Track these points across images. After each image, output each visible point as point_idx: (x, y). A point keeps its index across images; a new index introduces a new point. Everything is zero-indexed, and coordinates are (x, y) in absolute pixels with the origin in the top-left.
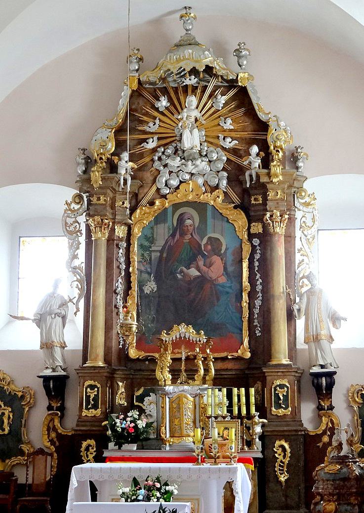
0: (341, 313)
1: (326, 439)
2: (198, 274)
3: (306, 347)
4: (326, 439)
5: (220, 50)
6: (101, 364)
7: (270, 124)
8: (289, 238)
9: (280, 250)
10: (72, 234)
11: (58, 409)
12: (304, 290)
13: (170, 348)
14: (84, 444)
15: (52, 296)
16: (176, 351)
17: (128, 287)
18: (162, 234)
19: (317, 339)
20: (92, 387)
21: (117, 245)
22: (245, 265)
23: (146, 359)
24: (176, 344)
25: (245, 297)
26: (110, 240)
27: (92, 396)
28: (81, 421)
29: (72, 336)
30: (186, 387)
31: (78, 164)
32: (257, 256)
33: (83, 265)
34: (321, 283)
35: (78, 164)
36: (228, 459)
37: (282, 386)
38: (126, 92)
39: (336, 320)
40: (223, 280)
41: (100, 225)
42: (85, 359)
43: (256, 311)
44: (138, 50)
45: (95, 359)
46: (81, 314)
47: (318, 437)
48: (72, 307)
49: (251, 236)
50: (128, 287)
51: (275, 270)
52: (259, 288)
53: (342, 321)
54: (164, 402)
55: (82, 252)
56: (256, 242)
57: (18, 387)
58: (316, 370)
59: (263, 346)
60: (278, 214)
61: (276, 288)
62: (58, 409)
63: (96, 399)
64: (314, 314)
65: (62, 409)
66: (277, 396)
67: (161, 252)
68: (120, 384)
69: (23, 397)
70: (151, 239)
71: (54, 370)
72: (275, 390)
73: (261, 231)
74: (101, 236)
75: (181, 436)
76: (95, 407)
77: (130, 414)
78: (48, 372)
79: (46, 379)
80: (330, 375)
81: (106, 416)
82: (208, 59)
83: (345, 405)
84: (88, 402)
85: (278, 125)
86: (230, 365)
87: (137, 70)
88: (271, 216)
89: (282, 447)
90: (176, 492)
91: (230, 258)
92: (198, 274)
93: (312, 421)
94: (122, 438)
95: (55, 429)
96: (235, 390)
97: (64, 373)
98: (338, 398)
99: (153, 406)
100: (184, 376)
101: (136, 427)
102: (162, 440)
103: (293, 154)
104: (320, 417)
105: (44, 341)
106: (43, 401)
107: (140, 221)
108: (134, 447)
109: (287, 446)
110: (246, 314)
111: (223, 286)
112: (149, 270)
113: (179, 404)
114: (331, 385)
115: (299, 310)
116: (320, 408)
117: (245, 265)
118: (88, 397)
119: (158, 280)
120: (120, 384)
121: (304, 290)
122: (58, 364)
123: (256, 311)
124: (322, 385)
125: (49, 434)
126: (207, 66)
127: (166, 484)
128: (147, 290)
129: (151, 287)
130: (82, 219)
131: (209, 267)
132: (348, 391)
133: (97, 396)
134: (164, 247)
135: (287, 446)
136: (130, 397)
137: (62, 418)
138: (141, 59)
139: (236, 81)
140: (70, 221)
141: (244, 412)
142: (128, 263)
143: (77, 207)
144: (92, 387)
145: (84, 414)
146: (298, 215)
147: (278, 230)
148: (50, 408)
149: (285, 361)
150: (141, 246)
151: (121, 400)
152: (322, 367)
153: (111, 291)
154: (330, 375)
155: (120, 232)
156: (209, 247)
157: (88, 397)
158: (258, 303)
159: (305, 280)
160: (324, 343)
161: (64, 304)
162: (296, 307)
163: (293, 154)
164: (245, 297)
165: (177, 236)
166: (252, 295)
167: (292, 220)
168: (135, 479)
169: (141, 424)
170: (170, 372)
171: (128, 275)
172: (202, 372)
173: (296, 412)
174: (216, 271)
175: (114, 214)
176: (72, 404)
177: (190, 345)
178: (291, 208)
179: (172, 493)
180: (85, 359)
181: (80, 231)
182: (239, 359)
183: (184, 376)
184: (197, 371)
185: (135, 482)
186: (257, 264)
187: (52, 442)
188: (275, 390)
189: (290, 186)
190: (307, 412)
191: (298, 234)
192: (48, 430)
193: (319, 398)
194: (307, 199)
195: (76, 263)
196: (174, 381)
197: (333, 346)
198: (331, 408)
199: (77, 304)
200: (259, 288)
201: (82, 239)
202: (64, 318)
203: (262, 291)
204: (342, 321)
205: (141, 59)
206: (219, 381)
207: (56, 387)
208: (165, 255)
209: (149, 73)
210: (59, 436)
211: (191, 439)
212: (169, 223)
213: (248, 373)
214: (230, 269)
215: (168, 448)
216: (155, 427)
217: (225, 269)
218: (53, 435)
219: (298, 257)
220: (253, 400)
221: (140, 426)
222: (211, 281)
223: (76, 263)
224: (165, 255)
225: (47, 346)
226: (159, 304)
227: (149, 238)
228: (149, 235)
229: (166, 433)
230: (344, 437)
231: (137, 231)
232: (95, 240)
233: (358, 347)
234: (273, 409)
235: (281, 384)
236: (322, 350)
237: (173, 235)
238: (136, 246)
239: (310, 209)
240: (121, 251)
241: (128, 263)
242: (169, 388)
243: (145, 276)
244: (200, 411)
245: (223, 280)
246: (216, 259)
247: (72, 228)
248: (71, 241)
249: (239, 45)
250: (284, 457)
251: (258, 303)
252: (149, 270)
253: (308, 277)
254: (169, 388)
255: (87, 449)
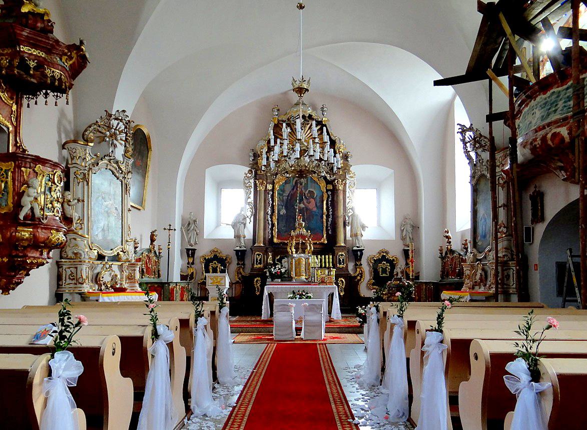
0: (366, 224)
1: (359, 278)
2: (304, 206)
3: (351, 239)
4: (359, 278)
5: (314, 109)
6: (262, 245)
7: (336, 141)
8: (344, 191)
9: (341, 197)
10: (249, 187)
11: (242, 264)
12: (350, 214)
13: (295, 238)
14: (256, 280)
15: (239, 215)
16: (297, 239)
17: (273, 211)
18: (288, 188)
19: (356, 235)
20: (259, 255)
21: (268, 193)
22: (325, 202)
23: (281, 243)
24: (298, 236)
25: (325, 217)
26: (265, 190)
27: (259, 259)
28: (253, 269)
29: (248, 232)
30: (302, 255)
31: (250, 156)
32: (330, 199)
33: (253, 202)
34: (357, 212)
35: (250, 156)
36: (331, 283)
37: (342, 255)
38: (272, 125)
39: (363, 227)
40: (315, 209)
41: (262, 184)
42: (254, 242)
43: (329, 223)
44: (277, 106)
45: (260, 243)
46: (252, 223)
47: (355, 277)
48: (248, 220)
49: (327, 191)
50: (273, 211)
51: (339, 206)
52: (331, 213)
53: (366, 228)
54: (292, 261)
55: (252, 196)
56: (330, 193)
57: (223, 255)
58: (355, 248)
59: (333, 237)
60: (341, 181)
61: (339, 213)
62: (242, 264)
63: (260, 260)
64: (355, 226)
65: (244, 264)
66: (339, 259)
67: (288, 196)
68: (270, 254)
69: (226, 259)
70: (283, 191)
71: (240, 247)
72: (339, 256)
73: (332, 188)
74: (261, 188)
75: (300, 276)
76: (260, 263)
77: (277, 266)
78: (238, 248)
79: (237, 251)
80: (361, 251)
81: (265, 267)
82: (309, 111)
83: (366, 264)
84: (257, 261)
85: (340, 142)
86: (318, 247)
87: (277, 115)
88: (337, 182)
89: (342, 281)
90: (312, 296)
91: (318, 200)
92: (304, 206)
93: (352, 270)
94: (274, 277)
95: (241, 273)
96: (327, 256)
97: (245, 249)
98: (364, 261)
99: (286, 263)
100: (300, 250)
101: (281, 272)
102: (291, 277)
103: (346, 155)
104: (356, 269)
105: (236, 235)
106: (235, 261)
107: (278, 182)
108: (280, 280)
109: (343, 280)
110: (325, 225)
111: (315, 212)
112: (282, 204)
113: (299, 263)
114: (362, 254)
115: (348, 223)
116: (356, 265)
117: (325, 202)
118: (257, 259)
119: (286, 208)
120: (270, 254)
121: (350, 214)
122: (243, 245)
123: (329, 223)
124: (356, 255)
125: (238, 276)
126: (309, 114)
127: (307, 293)
128: (281, 213)
129: (283, 211)
130: (252, 181)
131: (309, 203)
132: (368, 258)
133: (261, 259)
134: (289, 194)
135: (343, 280)
136: (274, 260)
137: (243, 268)
138: (279, 110)
139: (322, 121)
140: (246, 182)
141: (327, 266)
142: (273, 201)
143: (250, 175)
144: (259, 255)
145: (255, 267)
146: (348, 182)
147: (340, 188)
148: (238, 264)
149: (343, 244)
150: (278, 194)
151: (270, 261)
152: (358, 247)
153: (266, 213)
154: (361, 251)
155: (270, 187)
156: (309, 195)
157: (257, 259)
158: (330, 219)
159: (350, 210)
160: (359, 237)
161: (245, 219)
162: (347, 222)
163: (346, 155)
164: (325, 217)
165: (295, 189)
166: (328, 216)
167: (345, 184)
168: (293, 291)
169: (283, 270)
170: (294, 248)
171: (273, 206)
172: (309, 248)
173: (347, 266)
174: (312, 205)
175: (267, 179)
176: (248, 263)
177: (303, 237)
178: (344, 179)
179: (310, 297)
180: (254, 242)
181: (251, 186)
182: (322, 244)
183: (300, 250)
184: (307, 248)
185: (294, 293)
186: (330, 203)
187: (239, 279)
188: (339, 256)
189: (345, 169)
190: (351, 266)
191: (348, 190)
192: (238, 273)
193: (356, 261)
194: (352, 175)
195: (249, 200)
196: (296, 252)
197: (363, 238)
198: (361, 265)
199: (250, 219)
200: (331, 213)
201: (252, 190)
202: (245, 225)
203: (332, 215)
204: (366, 228)
205: (279, 110)
206: (315, 253)
207: (241, 255)
208: (289, 198)
209: (282, 116)
210: (242, 276)
211: (304, 277)
212: (291, 184)
213: (328, 248)
214: (318, 205)
215: (294, 281)
216: (288, 272)
217: (316, 205)
218: (240, 276)
219: (347, 200)
220: (331, 260)
221: (282, 272)
222: (310, 210)
223: (249, 200)
224: (289, 198)
225: (237, 237)
226: (287, 219)
227: (282, 190)
228: (282, 189)
229: (293, 274)
230: (399, 271)
231: (277, 187)
232: (259, 191)
233: (250, 238)
234: (338, 265)
235: (342, 255)
236: (358, 240)
237: (293, 189)
238: (277, 193)
239: (352, 179)
240: (270, 195)
241: (273, 201)
242: (295, 255)
243: (280, 207)
244: (308, 264)
245: (315, 209)
246: (312, 200)
247: (248, 185)
248: (247, 191)
249: (323, 105)
250: (343, 285)
251: (330, 219)
252: (282, 204)
253: (352, 209)
254: (295, 255)
255: (257, 281)
